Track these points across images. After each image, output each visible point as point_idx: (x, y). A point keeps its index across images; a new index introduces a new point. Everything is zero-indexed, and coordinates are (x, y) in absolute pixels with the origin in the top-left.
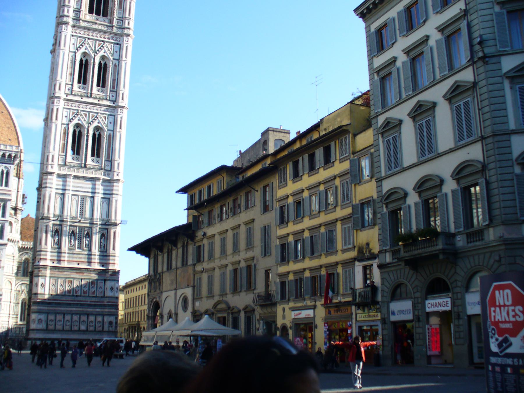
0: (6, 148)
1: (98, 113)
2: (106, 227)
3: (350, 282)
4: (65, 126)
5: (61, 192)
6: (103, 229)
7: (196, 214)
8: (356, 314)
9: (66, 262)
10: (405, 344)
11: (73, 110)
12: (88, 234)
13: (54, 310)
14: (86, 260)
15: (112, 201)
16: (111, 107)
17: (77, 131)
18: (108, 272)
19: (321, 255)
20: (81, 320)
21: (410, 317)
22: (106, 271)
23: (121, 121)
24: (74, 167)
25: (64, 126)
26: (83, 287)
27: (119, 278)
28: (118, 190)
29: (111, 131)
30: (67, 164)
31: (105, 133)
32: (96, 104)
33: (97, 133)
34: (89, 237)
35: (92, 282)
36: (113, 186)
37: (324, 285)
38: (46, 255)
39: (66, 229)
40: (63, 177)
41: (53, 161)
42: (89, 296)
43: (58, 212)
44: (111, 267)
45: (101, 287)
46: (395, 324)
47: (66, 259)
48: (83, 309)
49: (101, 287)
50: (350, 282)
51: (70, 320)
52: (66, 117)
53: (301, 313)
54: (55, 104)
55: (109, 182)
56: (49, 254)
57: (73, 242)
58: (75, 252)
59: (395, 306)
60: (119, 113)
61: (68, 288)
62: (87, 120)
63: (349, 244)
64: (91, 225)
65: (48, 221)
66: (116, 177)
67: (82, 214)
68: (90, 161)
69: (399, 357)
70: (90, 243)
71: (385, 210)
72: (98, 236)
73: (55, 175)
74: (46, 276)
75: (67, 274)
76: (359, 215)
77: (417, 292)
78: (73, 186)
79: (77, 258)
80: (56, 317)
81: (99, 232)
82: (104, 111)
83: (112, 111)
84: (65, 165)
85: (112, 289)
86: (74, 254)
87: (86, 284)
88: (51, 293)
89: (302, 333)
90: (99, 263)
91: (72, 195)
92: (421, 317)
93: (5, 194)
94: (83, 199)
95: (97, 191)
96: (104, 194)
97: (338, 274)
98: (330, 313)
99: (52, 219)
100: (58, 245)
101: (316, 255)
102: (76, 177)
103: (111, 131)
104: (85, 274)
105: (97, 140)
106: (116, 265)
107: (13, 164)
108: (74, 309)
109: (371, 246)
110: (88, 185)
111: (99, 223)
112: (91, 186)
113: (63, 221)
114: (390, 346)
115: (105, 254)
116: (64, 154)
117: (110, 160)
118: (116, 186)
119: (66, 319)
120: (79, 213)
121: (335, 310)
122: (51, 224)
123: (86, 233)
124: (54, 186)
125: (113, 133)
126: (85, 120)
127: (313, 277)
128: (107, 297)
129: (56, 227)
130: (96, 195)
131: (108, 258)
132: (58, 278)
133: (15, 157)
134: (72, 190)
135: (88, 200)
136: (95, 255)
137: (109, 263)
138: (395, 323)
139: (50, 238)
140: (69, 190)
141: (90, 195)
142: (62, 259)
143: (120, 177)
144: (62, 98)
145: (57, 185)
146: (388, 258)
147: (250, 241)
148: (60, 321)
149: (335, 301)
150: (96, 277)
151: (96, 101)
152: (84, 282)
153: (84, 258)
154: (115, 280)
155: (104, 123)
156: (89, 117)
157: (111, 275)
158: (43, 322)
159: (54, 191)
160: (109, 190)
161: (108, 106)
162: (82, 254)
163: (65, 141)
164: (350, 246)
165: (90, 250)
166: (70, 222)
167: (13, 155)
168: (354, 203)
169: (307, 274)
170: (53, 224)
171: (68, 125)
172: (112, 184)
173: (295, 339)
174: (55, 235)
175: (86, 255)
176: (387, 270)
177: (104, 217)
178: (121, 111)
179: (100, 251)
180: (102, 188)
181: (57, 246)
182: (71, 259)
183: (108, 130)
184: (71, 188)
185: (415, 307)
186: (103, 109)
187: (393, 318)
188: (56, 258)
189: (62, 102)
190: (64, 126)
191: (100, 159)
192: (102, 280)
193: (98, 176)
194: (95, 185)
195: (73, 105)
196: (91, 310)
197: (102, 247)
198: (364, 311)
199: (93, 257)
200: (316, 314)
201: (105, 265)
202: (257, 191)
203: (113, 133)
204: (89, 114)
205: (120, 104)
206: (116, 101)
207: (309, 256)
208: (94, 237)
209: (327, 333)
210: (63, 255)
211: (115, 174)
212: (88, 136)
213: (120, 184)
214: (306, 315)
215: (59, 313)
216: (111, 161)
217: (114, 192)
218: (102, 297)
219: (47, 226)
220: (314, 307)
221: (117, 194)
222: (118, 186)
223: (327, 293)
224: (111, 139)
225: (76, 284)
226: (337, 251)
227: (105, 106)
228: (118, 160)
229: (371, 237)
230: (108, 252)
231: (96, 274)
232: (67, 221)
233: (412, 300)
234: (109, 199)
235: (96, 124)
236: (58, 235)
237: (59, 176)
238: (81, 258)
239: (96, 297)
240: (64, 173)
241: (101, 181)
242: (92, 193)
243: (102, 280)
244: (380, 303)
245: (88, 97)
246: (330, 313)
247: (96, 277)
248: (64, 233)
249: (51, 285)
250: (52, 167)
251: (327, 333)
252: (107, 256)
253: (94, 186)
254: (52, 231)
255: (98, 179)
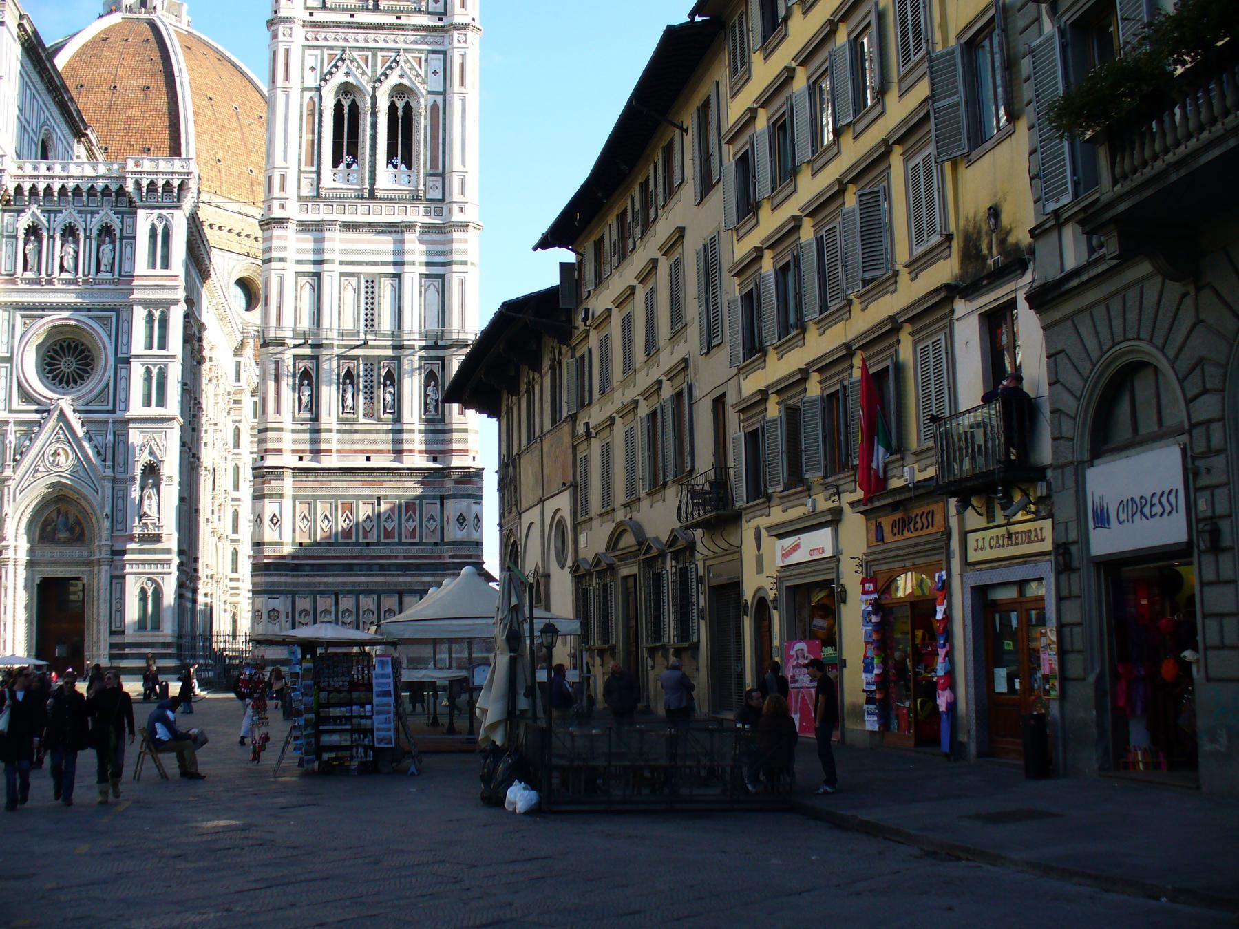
0: (157, 165)
1: (398, 51)
2: (440, 353)
3: (939, 392)
4: (312, 93)
5: (310, 268)
6: (431, 358)
7: (569, 256)
8: (964, 535)
9: (334, 454)
10: (1168, 669)
11: (331, 48)
12: (389, 375)
13: (309, 584)
14: (390, 447)
15: (450, 281)
16: (434, 29)
17: (346, 103)
18: (448, 476)
19: (850, 303)
20: (319, 610)
21: (1171, 530)
22: (442, 474)
23: (462, 65)
24: (342, 199)
25: (308, 95)
26: (383, 518)
27: (481, 489)
28: (465, 252)
29: (438, 93)
30: (323, 193)
31: (422, 100)
32: (391, 27)
33: (400, 105)
34: (392, 384)
35: (407, 504)
36: (451, 241)
37: (858, 421)
38: (280, 440)
39: (330, 367)
40: (315, 228)
41: (283, 189)
42: (400, 543)
43: (305, 323)
44: (456, 461)
45: (432, 517)
46: (1114, 568)
47: (334, 446)
48: (388, 579)
49: (432, 517)
50: (939, 392)
51: (354, 611)
52: (313, 69)
53: (798, 546)
54: (281, 37)
55: (440, 232)
56: (288, 437)
57: (349, 402)
58: (356, 427)
59: (1110, 481)
60: (456, 44)
61: (342, 524)
62: (369, 73)
63: (932, 232)
64: (397, 352)
65: (280, 349)
66: (457, 216)
67: (371, 323)
68: (386, 178)
69: (1138, 735)
70: (398, 398)
71: (1048, 26)
72: (416, 378)
73: (292, 227)
74: (281, 496)
75: (339, 486)
76: (959, 98)
77: (1205, 391)
78: (342, 252)
79: (362, 442)
80: (315, 602)
81: (420, 368)
82: (415, 42)
83: (439, 40)
84: (318, 195)
85: (461, 520)
86: (356, 431)
87: (392, 510)
88: (298, 540)
89: (819, 622)
90: (426, 452)
91: (342, 274)
92: (1225, 526)
93: (163, 287)
94: (372, 284)
95: (407, 258)
96: (428, 264)
97: (899, 368)
98: (880, 538)
99: (291, 342)
100: (311, 410)
101: (833, 306)
102: (349, 226)
103: (438, 93)
104: (387, 485)
105: (401, 124)
106: (471, 455)
107: (178, 207)
108: (363, 579)
109: (1005, 219)
110: (385, 243)
111: (417, 344)
112: (391, 247)
113: (318, 346)
114: (1092, 678)
115: (439, 427)
116: (314, 168)
117: (439, 172)
118: (460, 241)
119: (341, 608)
120: (362, 323)
121: (894, 524)
122: (288, 356)
123: (383, 373)
124: (292, 256)
125: (444, 101)
126: (364, 73)
127: (830, 396)
128: (449, 543)
129: (302, 365)
130: (407, 268)
131: (447, 436)
132: (316, 497)
133: (180, 187)
134: (341, 263)
135: (386, 286)
136: (412, 431)
137: (452, 451)
138: (1112, 566)
139: (287, 395)
140: (332, 262)
141: (391, 269)
142: (324, 446)
143: (471, 215)
144: (298, 22)
145: (299, 251)
146: (1072, 250)
147: (678, 310)
148: (327, 612)
149: (895, 483)
150: (419, 490)
151: (390, 19)
152: (384, 506)
153: (383, 442)
154: (468, 496)
155: (418, 75)
156: (375, 65)
157: (457, 482)
158: (283, 617)
159: (291, 269)
160: (442, 254)
161: (425, 28)
162: (377, 431)
163: (313, 133)
164: (936, 239)
165: (398, 419)
166: (339, 346)
167: (176, 183)
168: (939, 48)
169: (814, 388)
170: (295, 357)
171: (319, 89)
172: (448, 236)
173: (789, 648)
174: (301, 385)
175: (387, 431)
176: (1069, 307)
177: (433, 326)
178: (462, 38)
179: (427, 420)
180: (424, 248)
181: (308, 415)
182: (347, 447)
183: (430, 93)
184: (338, 257)
185: (1196, 474)
186: (412, 38)
187: (1103, 543)
188: (307, 447)
189: (299, 32)
190: (308, 95)
191: (413, 173)
192: (434, 497)
193: (408, 218)
194: (402, 242)
195: (331, 36)
196: (409, 579)
197: (431, 407)
198: (991, 517)
199: (406, 436)
200: (841, 546)
201: (439, 457)
202: (686, 131)
203: (444, 101)
204: (374, 56)
205: (458, 19)
206: (445, 13)
207: (816, 316)
208: (406, 382)
209: (874, 619)
210: (324, 435)
211: (455, 207)
212: (374, 114)
213: (471, 234)
214: (812, 552)
215: (322, 592)
216: (443, 176)
217: (455, 257)
218: (436, 544)
219: (277, 363)
220: (834, 519)
221: (465, 263)
222: (466, 241)
223: (869, 454)
224: (439, 114)
225: (364, 511)
226: (896, 274)
227: (416, 28)
228: (461, 168)
229: (1004, 179)
230: (447, 421)
231: (418, 482)
232: (331, 346)
233: (1184, 438)
234: (442, 276)
235: (394, 79)
236: (310, 384)
237: (304, 227)
238: (375, 441)
239: (421, 543)
240: (317, 218)
241: (418, 229)
242: (395, 264)
243: (434, 497)
244: (1049, 473)
245: (367, 9)
246: (880, 538)
247: (419, 490)
248: (324, 376)
249: (298, 519)
250: (282, 206)
251: (874, 619)
252: (444, 432)
253: (398, 247)
254: (294, 376)
255: (410, 226)
